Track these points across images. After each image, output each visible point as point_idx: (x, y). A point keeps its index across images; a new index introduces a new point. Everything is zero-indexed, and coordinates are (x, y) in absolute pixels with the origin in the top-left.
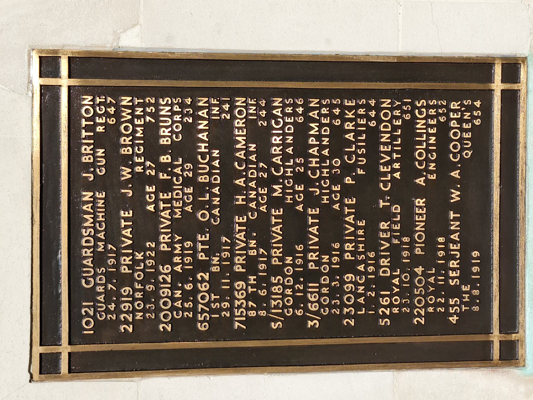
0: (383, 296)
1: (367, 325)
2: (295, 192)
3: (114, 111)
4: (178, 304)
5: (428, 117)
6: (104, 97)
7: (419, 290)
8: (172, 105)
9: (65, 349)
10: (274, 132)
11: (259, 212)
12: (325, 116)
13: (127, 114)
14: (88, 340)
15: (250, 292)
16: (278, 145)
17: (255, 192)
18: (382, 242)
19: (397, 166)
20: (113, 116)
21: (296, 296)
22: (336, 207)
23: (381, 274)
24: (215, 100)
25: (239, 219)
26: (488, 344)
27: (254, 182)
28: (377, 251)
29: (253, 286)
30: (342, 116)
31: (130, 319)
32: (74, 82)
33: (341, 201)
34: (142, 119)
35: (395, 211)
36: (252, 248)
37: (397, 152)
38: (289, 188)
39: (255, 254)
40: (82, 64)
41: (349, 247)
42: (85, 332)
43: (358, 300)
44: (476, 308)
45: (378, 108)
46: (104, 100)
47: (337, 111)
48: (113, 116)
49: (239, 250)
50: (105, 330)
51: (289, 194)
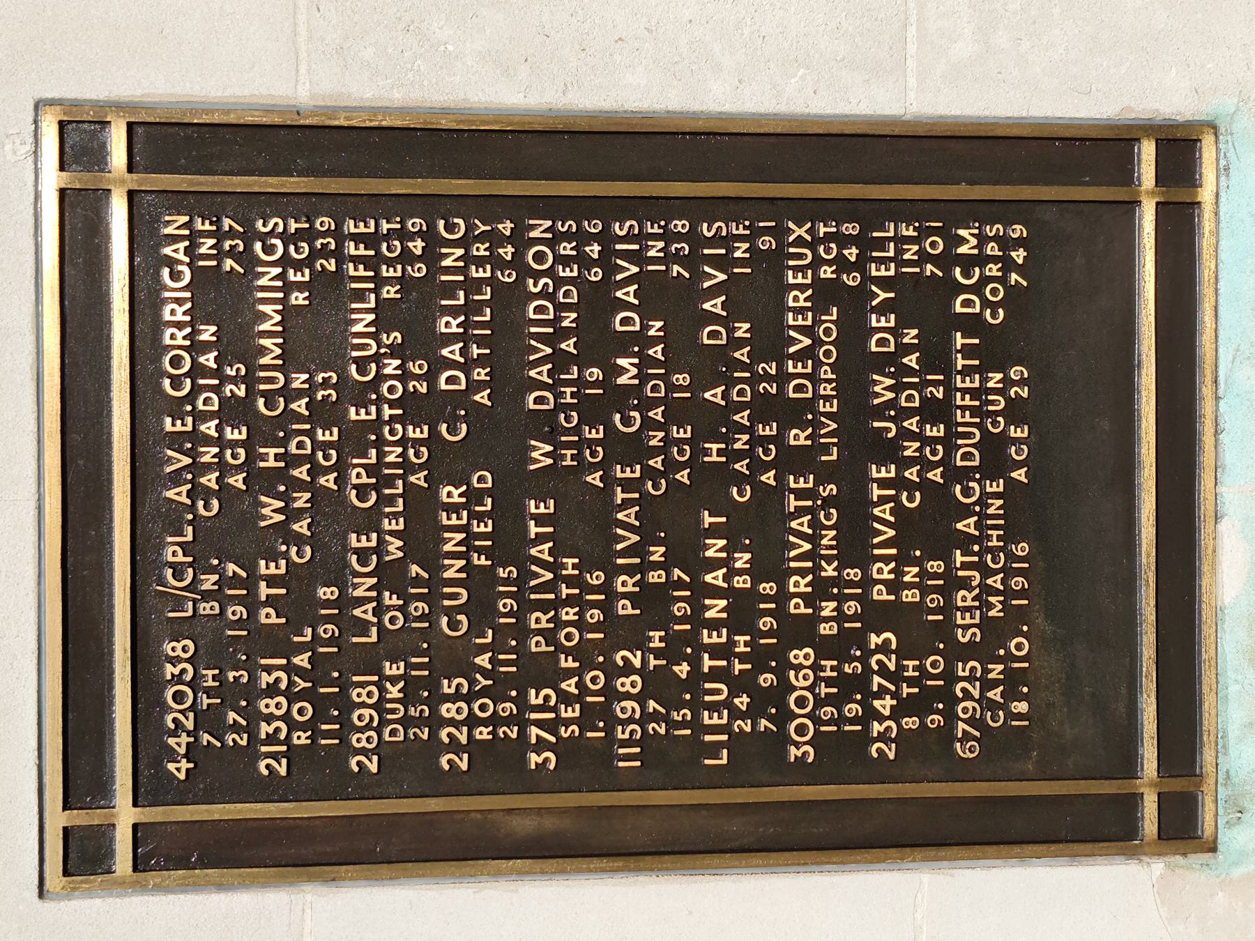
1: (761, 756)
5: (285, 261)
6: (398, 219)
7: (968, 667)
10: (167, 294)
11: (758, 487)
16: (179, 325)
19: (480, 374)
22: (595, 479)
24: (207, 222)
25: (449, 519)
26: (1134, 800)
29: (658, 654)
31: (463, 739)
32: (134, 181)
33: (605, 466)
39: (663, 580)
41: (883, 571)
45: (520, 240)
46: (399, 226)
51: (568, 445)
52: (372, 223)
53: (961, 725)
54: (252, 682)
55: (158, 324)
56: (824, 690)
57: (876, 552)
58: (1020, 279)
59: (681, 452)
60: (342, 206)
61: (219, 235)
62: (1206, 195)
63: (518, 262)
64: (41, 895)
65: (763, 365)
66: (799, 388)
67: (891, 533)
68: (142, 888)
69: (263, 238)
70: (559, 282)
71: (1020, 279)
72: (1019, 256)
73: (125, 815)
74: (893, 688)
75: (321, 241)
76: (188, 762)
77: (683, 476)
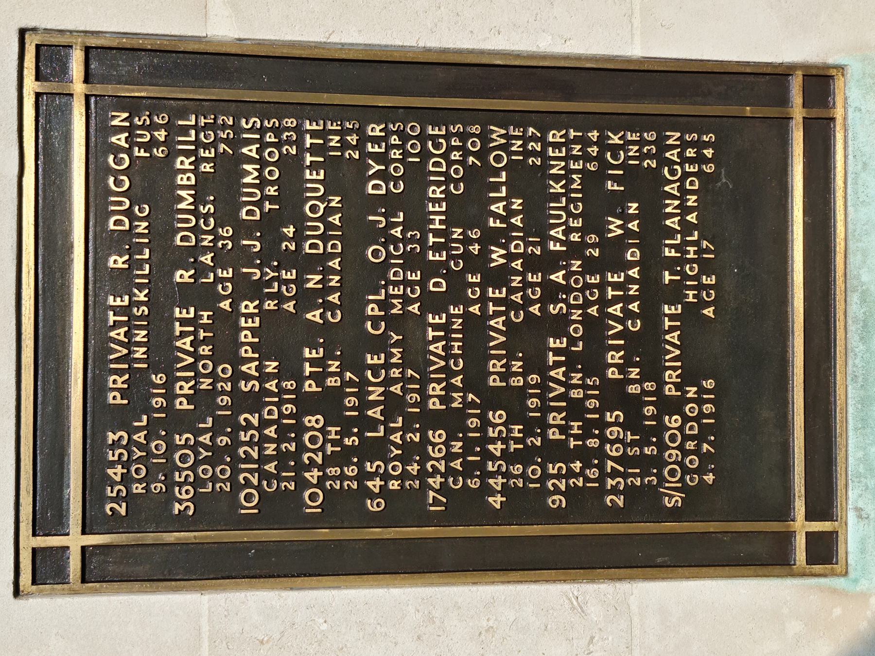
1: (644, 502)
2: (700, 287)
4: (271, 467)
8: (262, 131)
9: (74, 540)
14: (113, 524)
15: (329, 453)
20: (595, 159)
26: (788, 537)
27: (519, 262)
29: (576, 437)
34: (213, 150)
36: (516, 374)
38: (691, 278)
40: (111, 57)
42: (243, 511)
43: (452, 464)
44: (709, 478)
46: (212, 121)
48: (595, 159)
50: (149, 511)
52: (322, 122)
53: (431, 494)
57: (178, 374)
60: (302, 111)
61: (526, 140)
62: (839, 113)
63: (600, 158)
66: (313, 246)
67: (678, 352)
69: (433, 138)
72: (709, 153)
73: (74, 540)
74: (622, 469)
75: (287, 134)
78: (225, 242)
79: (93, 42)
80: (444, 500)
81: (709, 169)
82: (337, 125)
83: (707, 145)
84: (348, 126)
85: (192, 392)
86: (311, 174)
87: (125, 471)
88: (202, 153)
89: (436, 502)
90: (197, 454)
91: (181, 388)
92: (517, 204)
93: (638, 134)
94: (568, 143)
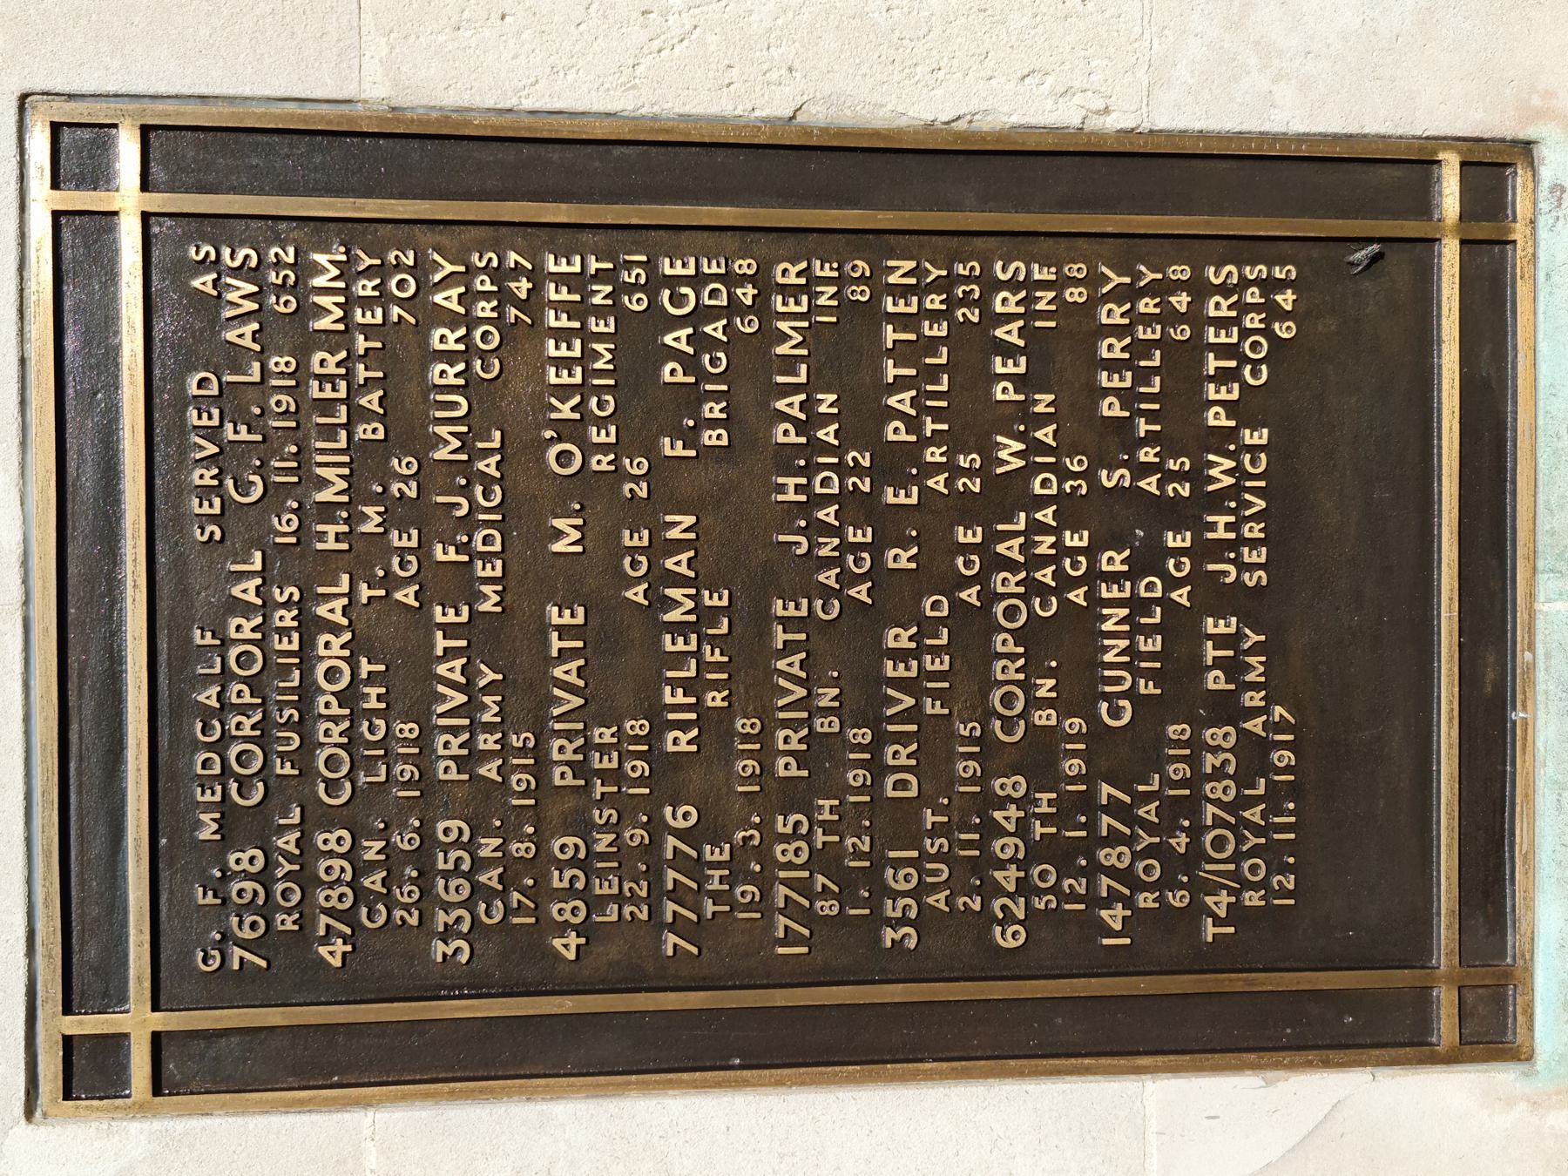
0: (898, 864)
1: (850, 949)
3: (754, 297)
9: (138, 1021)
12: (1148, 320)
13: (243, 297)
17: (836, 541)
18: (890, 692)
21: (192, 888)
23: (890, 793)
26: (1422, 1000)
27: (1050, 511)
28: (875, 722)
29: (828, 828)
30: (1196, 317)
32: (158, 202)
35: (1148, 595)
37: (1151, 416)
40: (190, 146)
47: (1181, 301)
49: (560, 718)
54: (307, 741)
55: (182, 490)
56: (1038, 830)
58: (1286, 715)
59: (858, 562)
62: (1519, 233)
64: (29, 1113)
65: (964, 310)
68: (155, 1113)
70: (1245, 333)
71: (1286, 715)
72: (1286, 299)
73: (138, 1021)
76: (345, 943)
77: (860, 592)
78: (1075, 484)
79: (157, 115)
80: (806, 932)
81: (1285, 330)
82: (832, 269)
83: (1282, 285)
84: (961, 271)
85: (465, 752)
86: (1004, 365)
87: (1022, 874)
88: (1142, 333)
89: (790, 938)
90: (1240, 840)
91: (446, 745)
92: (827, 402)
93: (1053, 270)
94: (810, 285)
